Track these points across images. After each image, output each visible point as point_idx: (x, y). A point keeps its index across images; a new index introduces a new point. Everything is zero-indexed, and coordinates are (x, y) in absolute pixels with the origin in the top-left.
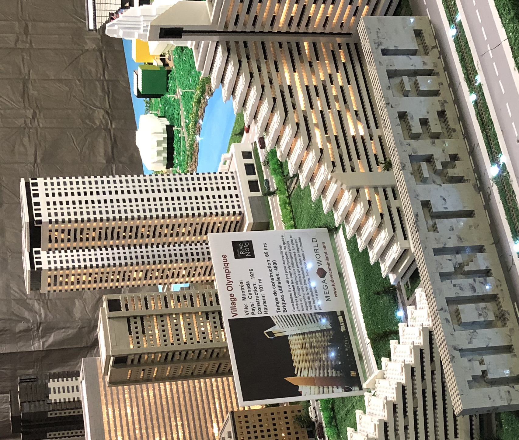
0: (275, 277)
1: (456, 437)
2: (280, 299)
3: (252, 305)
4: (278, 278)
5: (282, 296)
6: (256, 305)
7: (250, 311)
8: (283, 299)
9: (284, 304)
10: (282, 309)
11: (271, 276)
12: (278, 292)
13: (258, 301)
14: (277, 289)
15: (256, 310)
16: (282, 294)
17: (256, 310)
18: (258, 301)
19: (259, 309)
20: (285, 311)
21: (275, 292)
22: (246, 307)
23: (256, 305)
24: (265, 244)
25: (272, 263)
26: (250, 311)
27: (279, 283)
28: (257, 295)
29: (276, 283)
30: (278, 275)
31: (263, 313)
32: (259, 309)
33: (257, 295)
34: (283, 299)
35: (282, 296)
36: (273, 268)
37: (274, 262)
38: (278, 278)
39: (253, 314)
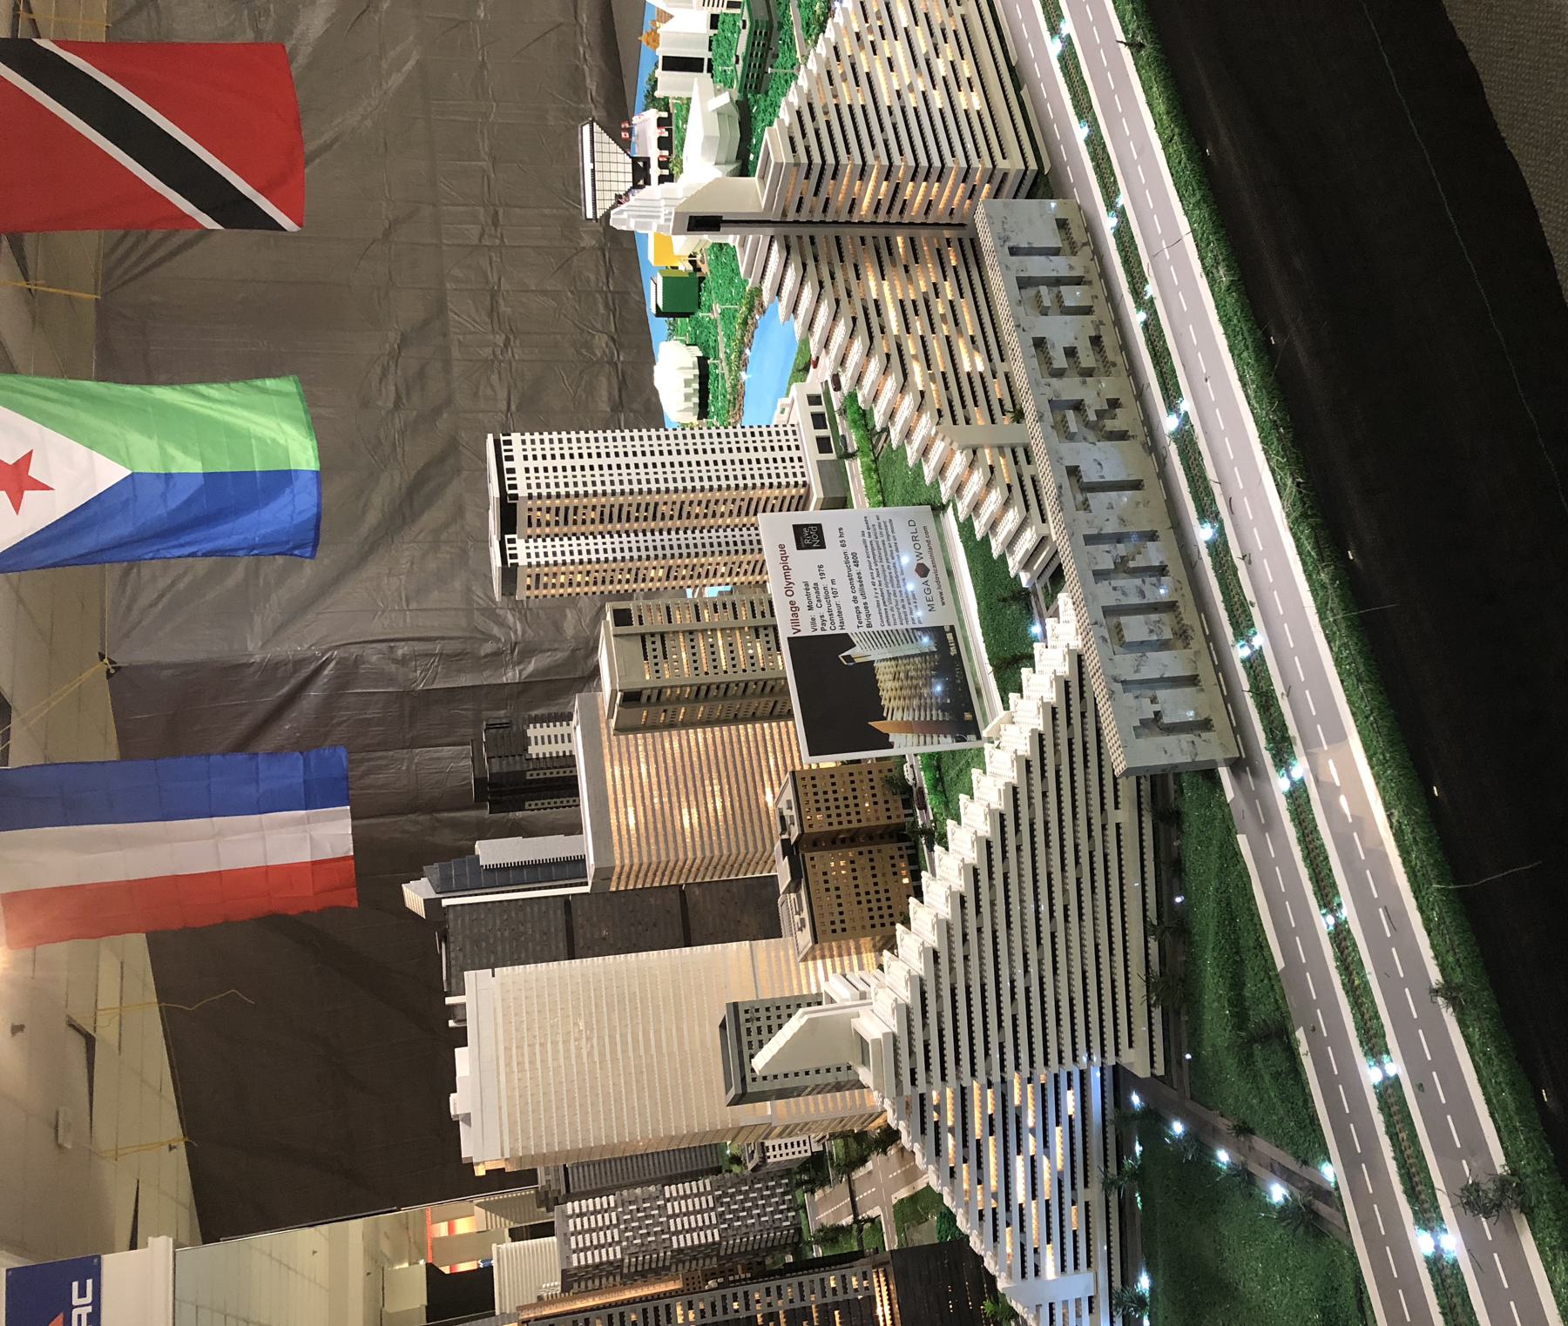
0: (855, 577)
1: (1117, 807)
2: (862, 609)
6: (827, 617)
7: (819, 626)
8: (866, 608)
9: (868, 616)
10: (865, 623)
11: (850, 575)
12: (860, 598)
13: (830, 611)
14: (858, 594)
15: (828, 624)
17: (828, 624)
18: (830, 611)
19: (833, 623)
20: (869, 626)
21: (855, 598)
22: (813, 619)
23: (827, 617)
26: (819, 626)
28: (829, 603)
29: (857, 585)
31: (838, 628)
32: (833, 623)
33: (829, 603)
34: (866, 608)
36: (852, 564)
37: (854, 555)
39: (823, 629)
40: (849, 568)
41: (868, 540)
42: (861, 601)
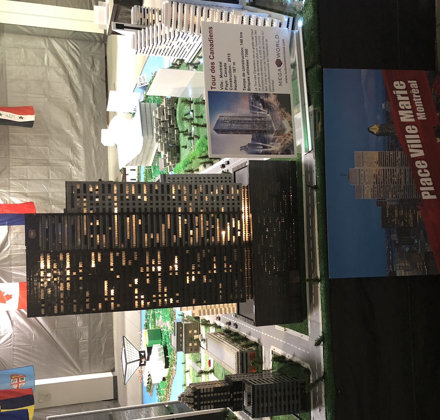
3: (226, 82)
4: (248, 63)
5: (249, 77)
6: (229, 83)
8: (249, 80)
9: (249, 84)
10: (247, 88)
12: (246, 74)
16: (248, 76)
20: (249, 90)
22: (222, 83)
24: (241, 33)
25: (244, 51)
26: (224, 87)
27: (248, 67)
28: (231, 75)
31: (234, 89)
33: (231, 75)
34: (249, 80)
35: (249, 77)
37: (246, 50)
38: (248, 63)
40: (243, 57)
41: (257, 76)
42: (246, 76)
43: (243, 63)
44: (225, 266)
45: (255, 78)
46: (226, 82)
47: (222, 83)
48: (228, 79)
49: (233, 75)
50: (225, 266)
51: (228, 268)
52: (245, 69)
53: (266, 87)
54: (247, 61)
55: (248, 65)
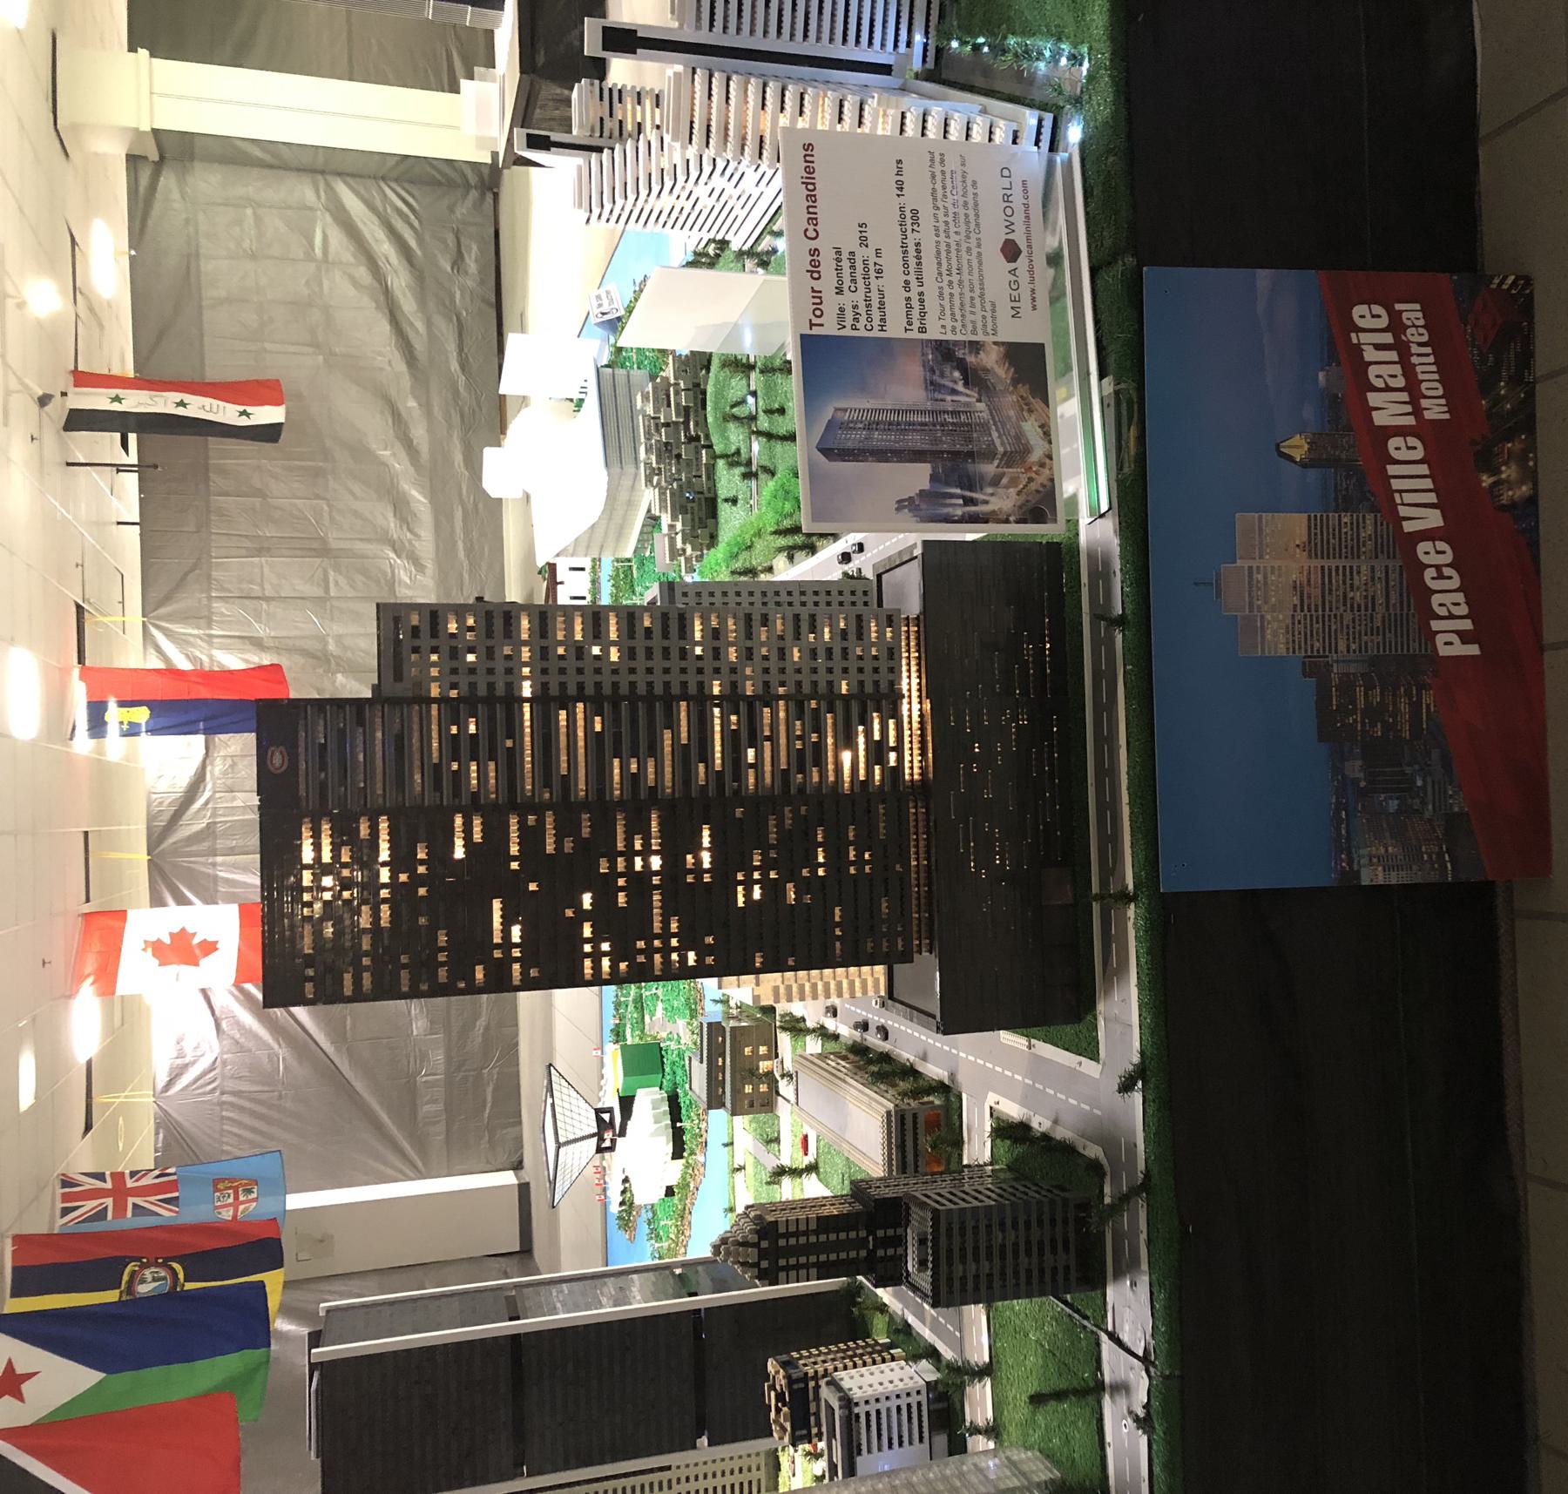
3: (855, 307)
4: (918, 251)
5: (921, 294)
6: (862, 310)
7: (849, 321)
8: (922, 301)
9: (923, 314)
10: (916, 324)
11: (904, 246)
13: (867, 299)
16: (921, 289)
20: (922, 330)
22: (842, 310)
23: (862, 310)
26: (849, 321)
27: (919, 264)
28: (868, 286)
30: (918, 244)
31: (876, 328)
33: (868, 286)
34: (922, 301)
35: (921, 294)
37: (915, 212)
38: (918, 251)
40: (904, 233)
41: (947, 291)
42: (915, 288)
43: (905, 252)
44: (852, 854)
45: (941, 295)
46: (855, 307)
47: (842, 310)
48: (859, 297)
49: (873, 287)
50: (852, 854)
51: (860, 862)
52: (911, 269)
53: (973, 322)
54: (918, 244)
55: (918, 258)
